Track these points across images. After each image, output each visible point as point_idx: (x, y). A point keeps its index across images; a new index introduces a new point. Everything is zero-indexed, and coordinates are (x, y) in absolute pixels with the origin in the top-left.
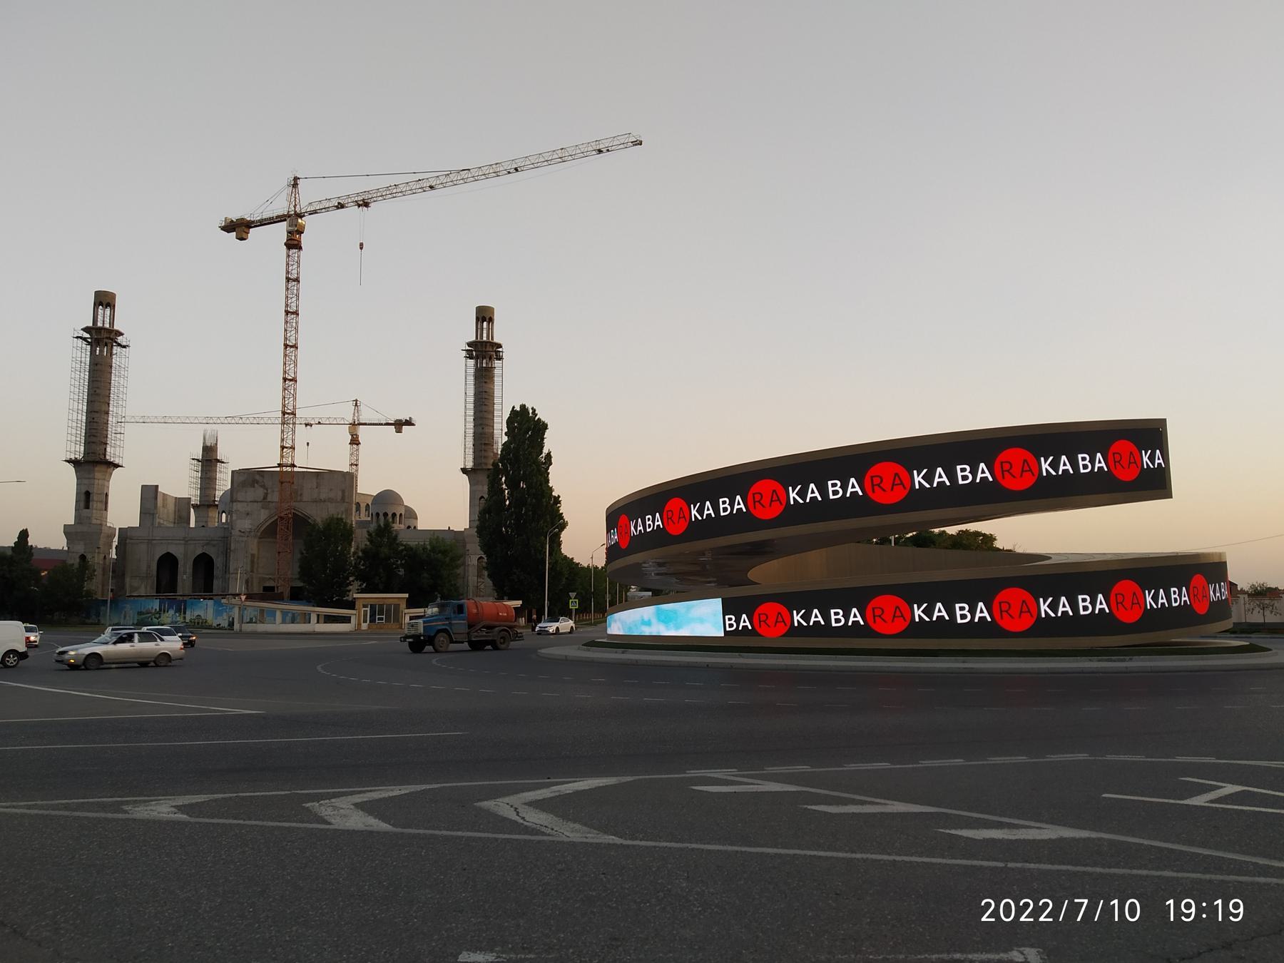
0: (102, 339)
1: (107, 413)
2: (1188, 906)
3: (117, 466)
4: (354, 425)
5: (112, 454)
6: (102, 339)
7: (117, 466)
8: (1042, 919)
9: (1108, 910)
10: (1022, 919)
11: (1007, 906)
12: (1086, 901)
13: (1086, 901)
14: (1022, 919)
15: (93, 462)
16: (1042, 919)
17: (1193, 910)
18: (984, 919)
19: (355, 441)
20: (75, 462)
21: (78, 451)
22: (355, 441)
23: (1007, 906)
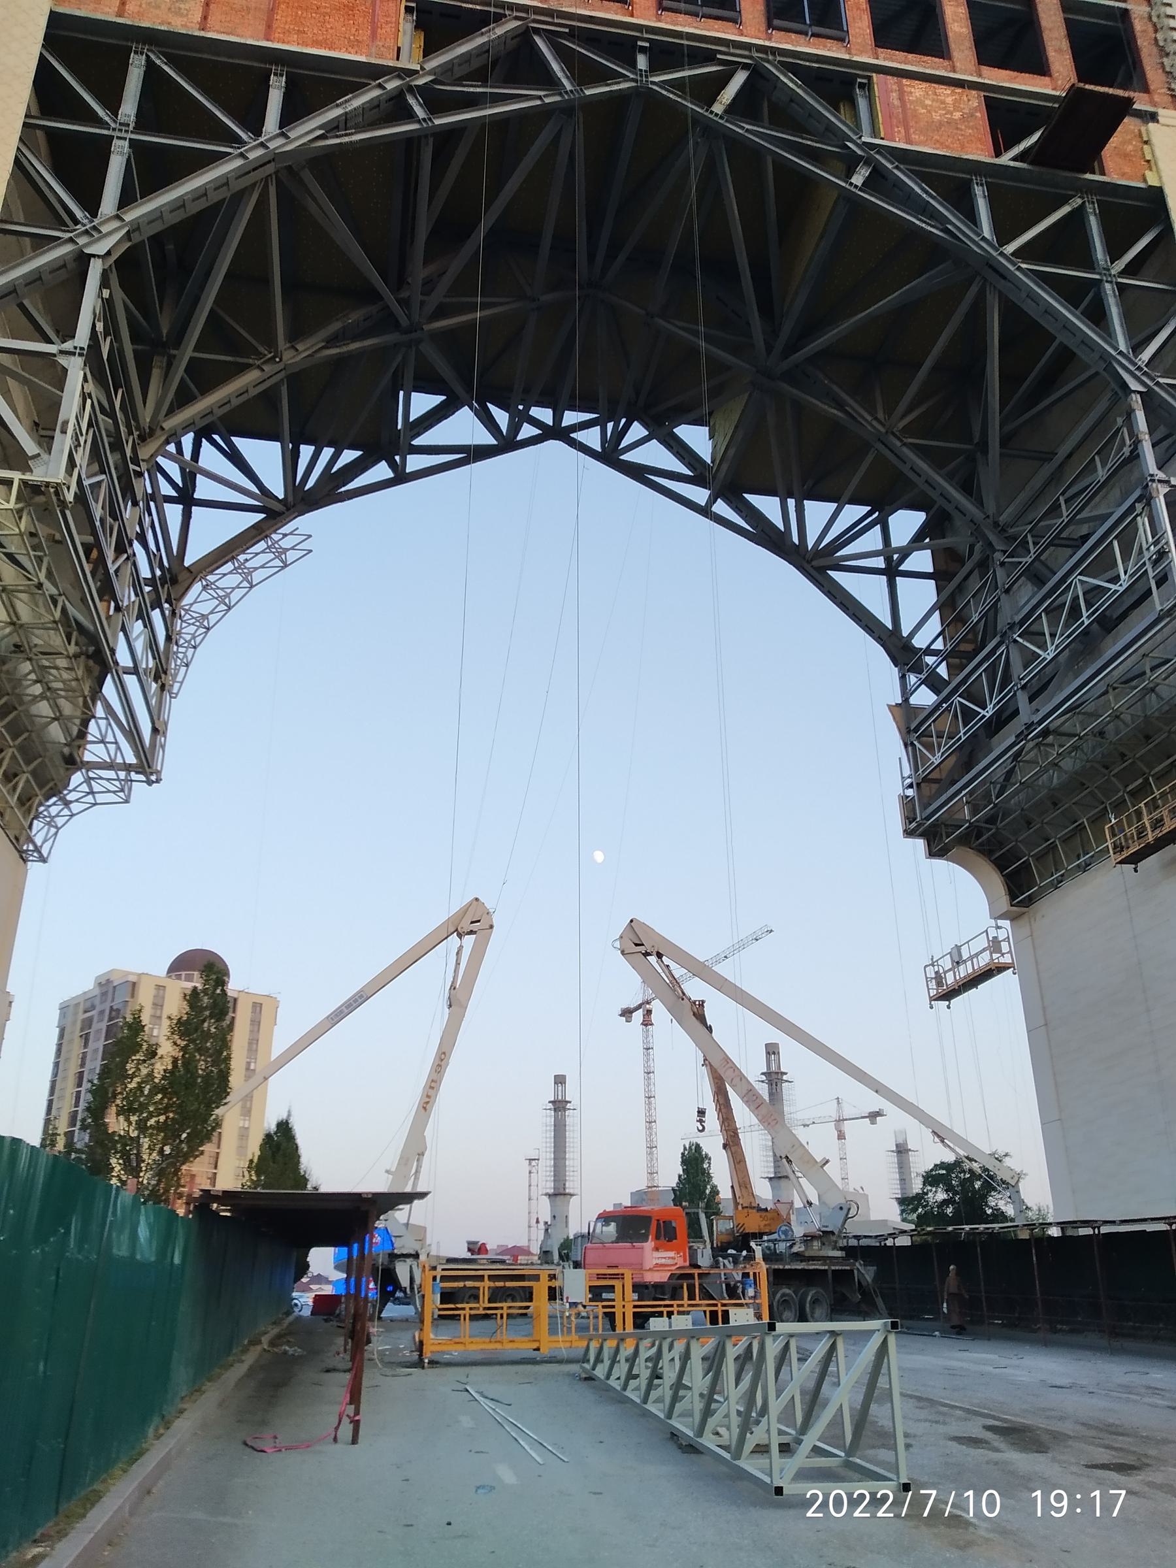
0: (559, 1106)
1: (565, 1159)
2: (1059, 1498)
3: (572, 1195)
4: (840, 1121)
5: (570, 1187)
6: (559, 1106)
7: (572, 1195)
8: (880, 1514)
9: (960, 1504)
10: (856, 1514)
11: (838, 1499)
12: (934, 1492)
13: (934, 1492)
14: (856, 1514)
15: (559, 1194)
16: (880, 1514)
17: (1065, 1503)
18: (809, 1514)
19: (841, 1136)
20: (550, 1196)
21: (550, 1188)
22: (841, 1136)
23: (838, 1499)
